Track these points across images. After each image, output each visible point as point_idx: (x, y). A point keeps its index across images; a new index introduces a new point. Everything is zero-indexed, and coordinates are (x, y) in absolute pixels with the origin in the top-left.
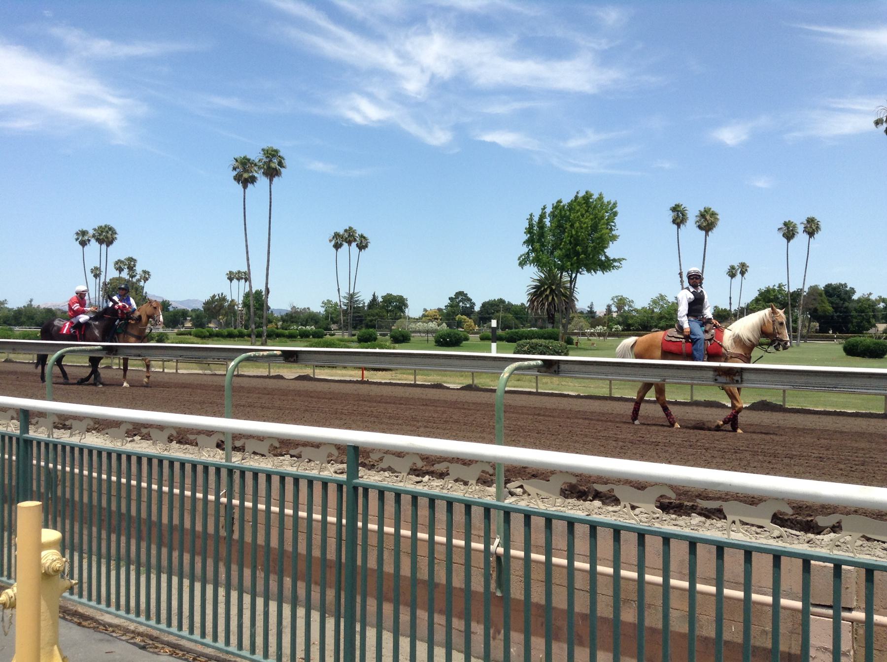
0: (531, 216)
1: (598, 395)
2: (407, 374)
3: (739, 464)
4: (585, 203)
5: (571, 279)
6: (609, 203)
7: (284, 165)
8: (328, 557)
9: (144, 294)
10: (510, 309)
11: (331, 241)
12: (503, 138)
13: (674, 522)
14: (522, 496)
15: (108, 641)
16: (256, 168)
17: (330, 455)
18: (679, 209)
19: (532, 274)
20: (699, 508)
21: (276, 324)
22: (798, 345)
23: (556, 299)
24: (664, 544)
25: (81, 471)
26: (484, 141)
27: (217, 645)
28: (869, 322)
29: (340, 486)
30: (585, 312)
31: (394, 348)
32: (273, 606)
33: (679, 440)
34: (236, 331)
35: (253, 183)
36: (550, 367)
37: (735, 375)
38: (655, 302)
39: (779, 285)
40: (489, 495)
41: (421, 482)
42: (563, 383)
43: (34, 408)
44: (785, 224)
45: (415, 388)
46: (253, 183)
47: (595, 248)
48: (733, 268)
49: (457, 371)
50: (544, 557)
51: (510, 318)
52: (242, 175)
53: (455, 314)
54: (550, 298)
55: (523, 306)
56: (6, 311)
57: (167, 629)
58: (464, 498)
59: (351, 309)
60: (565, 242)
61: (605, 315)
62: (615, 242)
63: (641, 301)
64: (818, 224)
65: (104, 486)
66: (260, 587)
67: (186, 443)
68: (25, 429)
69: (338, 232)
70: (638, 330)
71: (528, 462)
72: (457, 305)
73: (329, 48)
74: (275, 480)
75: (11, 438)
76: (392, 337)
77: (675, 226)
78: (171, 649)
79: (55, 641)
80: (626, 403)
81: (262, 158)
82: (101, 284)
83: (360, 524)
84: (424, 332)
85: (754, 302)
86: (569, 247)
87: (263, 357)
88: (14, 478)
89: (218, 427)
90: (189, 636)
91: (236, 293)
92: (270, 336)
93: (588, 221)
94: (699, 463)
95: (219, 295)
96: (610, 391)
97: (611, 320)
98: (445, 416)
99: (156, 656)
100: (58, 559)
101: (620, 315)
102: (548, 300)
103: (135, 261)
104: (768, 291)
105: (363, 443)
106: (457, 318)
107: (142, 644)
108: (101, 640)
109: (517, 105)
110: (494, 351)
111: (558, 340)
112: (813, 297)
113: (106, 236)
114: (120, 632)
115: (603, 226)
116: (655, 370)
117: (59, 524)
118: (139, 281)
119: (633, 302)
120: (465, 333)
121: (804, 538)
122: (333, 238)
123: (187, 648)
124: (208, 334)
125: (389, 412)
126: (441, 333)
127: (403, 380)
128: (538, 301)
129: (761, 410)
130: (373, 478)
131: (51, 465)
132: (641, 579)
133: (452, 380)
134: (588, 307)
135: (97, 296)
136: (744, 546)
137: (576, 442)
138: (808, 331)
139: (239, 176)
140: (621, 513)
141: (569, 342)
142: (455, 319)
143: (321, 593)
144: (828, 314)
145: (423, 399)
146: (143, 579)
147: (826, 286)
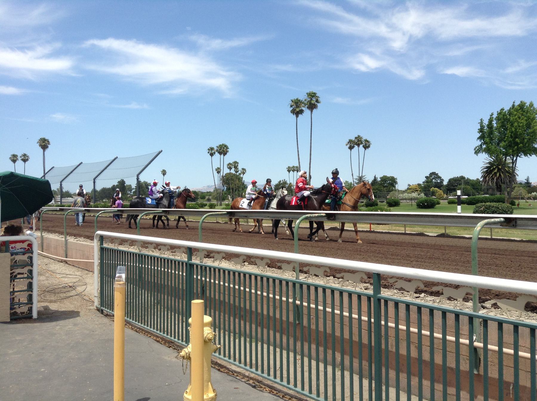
0: (481, 121)
2: (399, 227)
10: (468, 182)
11: (346, 145)
12: (459, 71)
14: (491, 309)
15: (235, 381)
16: (303, 105)
17: (325, 271)
23: (502, 175)
25: (215, 281)
26: (447, 74)
27: (297, 389)
30: (523, 183)
31: (390, 211)
36: (510, 223)
40: (468, 308)
42: (510, 232)
45: (405, 236)
47: (530, 139)
51: (469, 189)
54: (498, 175)
55: (478, 181)
57: (268, 377)
60: (508, 137)
66: (321, 356)
67: (273, 267)
68: (190, 258)
69: (351, 139)
71: (492, 286)
73: (344, 28)
74: (328, 292)
75: (183, 263)
78: (270, 389)
79: (210, 380)
82: (221, 177)
83: (383, 323)
84: (409, 199)
88: (184, 285)
89: (266, 256)
90: (280, 382)
98: (429, 254)
99: (261, 392)
100: (211, 333)
102: (496, 176)
103: (238, 163)
105: (383, 272)
106: (431, 190)
107: (254, 384)
108: (232, 381)
109: (469, 49)
110: (459, 211)
111: (504, 203)
116: (427, 219)
117: (212, 314)
118: (240, 174)
120: (438, 199)
122: (348, 143)
123: (279, 389)
125: (391, 251)
126: (420, 199)
127: (396, 230)
128: (489, 177)
130: (387, 293)
134: (525, 180)
135: (219, 183)
136: (406, 302)
137: (524, 272)
141: (513, 204)
142: (430, 190)
145: (412, 243)
146: (254, 344)
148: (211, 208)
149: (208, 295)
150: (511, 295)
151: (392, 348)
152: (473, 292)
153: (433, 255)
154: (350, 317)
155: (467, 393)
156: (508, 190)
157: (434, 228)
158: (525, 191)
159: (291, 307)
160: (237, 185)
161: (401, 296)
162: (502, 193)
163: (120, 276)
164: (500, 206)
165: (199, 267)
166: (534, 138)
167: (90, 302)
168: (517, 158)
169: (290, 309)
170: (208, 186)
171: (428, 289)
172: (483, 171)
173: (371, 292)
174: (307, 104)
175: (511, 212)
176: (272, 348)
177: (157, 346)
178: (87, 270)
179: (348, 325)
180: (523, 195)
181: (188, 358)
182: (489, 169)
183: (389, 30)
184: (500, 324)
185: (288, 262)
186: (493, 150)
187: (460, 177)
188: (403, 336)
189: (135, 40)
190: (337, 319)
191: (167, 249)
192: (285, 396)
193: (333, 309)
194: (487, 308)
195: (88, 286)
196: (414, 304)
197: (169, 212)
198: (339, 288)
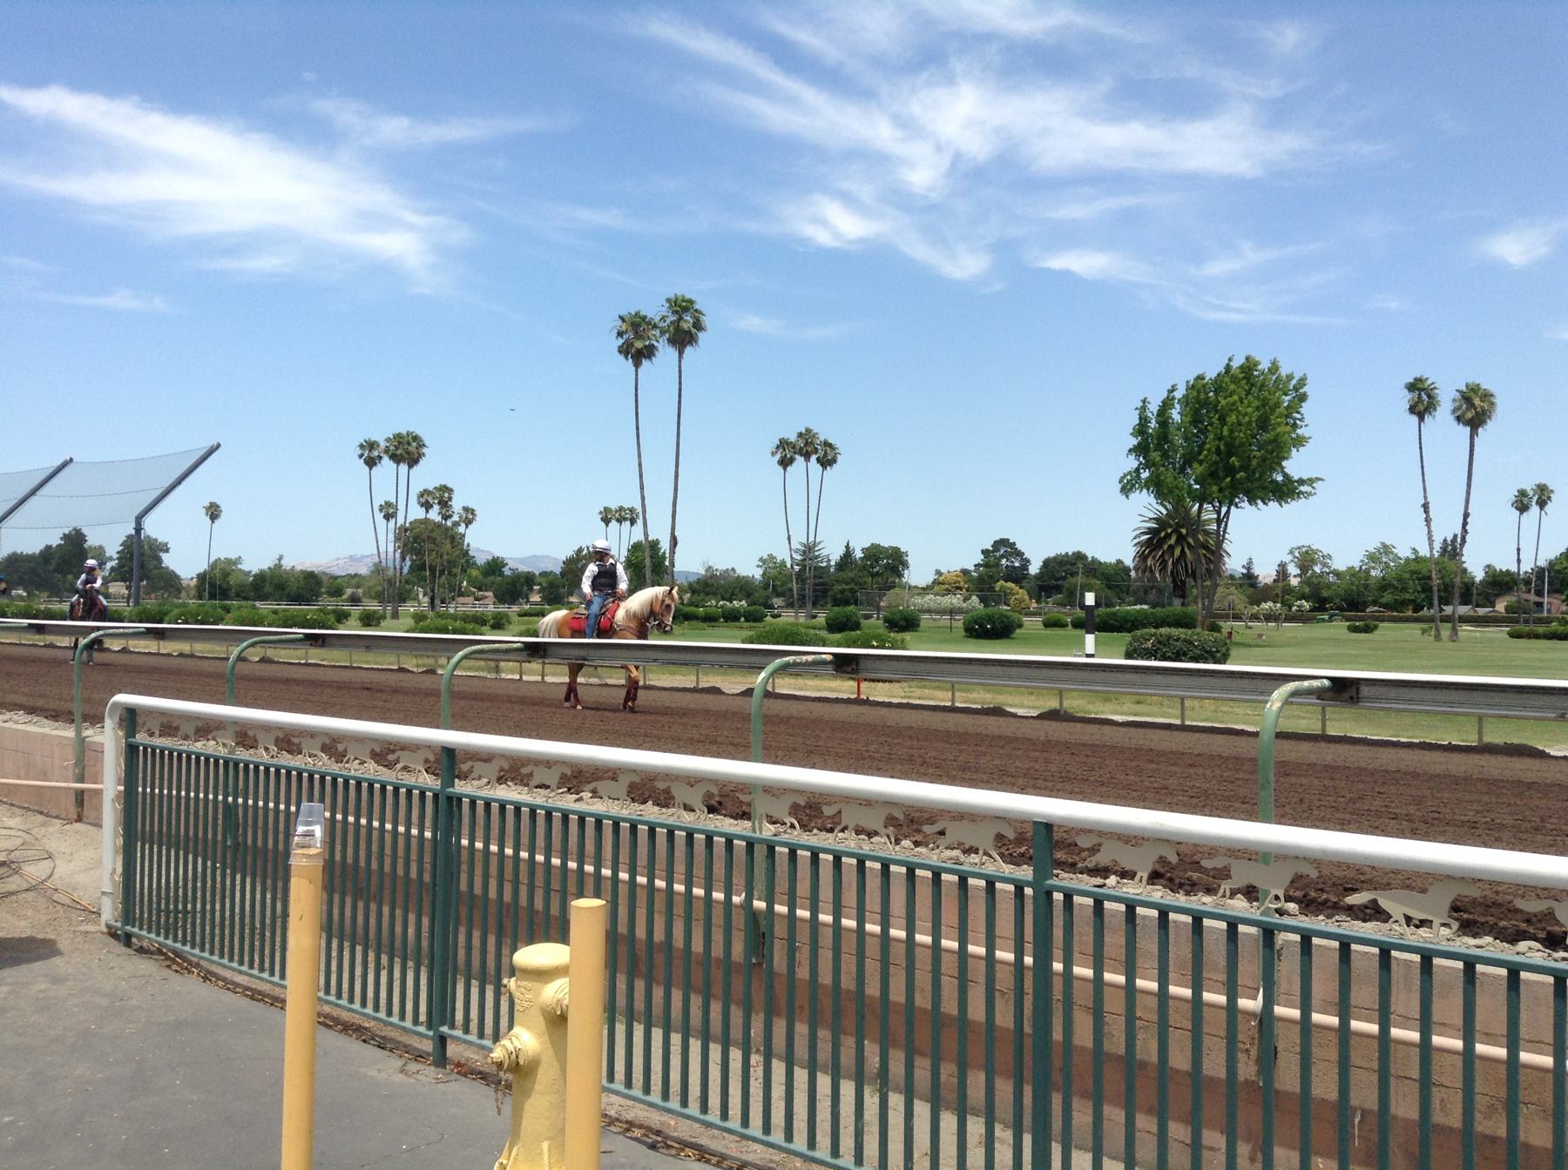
2: (929, 689)
4: (1246, 377)
6: (1290, 377)
11: (773, 454)
12: (1084, 263)
16: (657, 333)
18: (1421, 386)
19: (1145, 507)
26: (1049, 269)
38: (1372, 557)
41: (1105, 885)
47: (1264, 459)
48: (1522, 493)
49: (1025, 687)
52: (632, 345)
53: (993, 579)
54: (1177, 552)
56: (242, 577)
60: (1209, 450)
61: (1275, 581)
62: (1301, 449)
66: (801, 1050)
72: (998, 565)
73: (775, 117)
76: (886, 620)
77: (1415, 419)
78: (696, 1152)
85: (1564, 558)
87: (807, 664)
93: (1250, 410)
96: (1324, 726)
97: (1288, 590)
101: (1306, 582)
102: (1173, 554)
103: (450, 491)
105: (1063, 818)
106: (998, 586)
113: (407, 451)
115: (1279, 420)
118: (456, 524)
119: (1330, 557)
122: (778, 447)
126: (975, 613)
128: (1154, 557)
133: (1016, 700)
134: (1243, 567)
140: (1492, 949)
142: (993, 588)
157: (1022, 694)
158: (1243, 598)
159: (739, 920)
160: (445, 557)
163: (307, 831)
167: (78, 912)
172: (1137, 540)
174: (668, 331)
175: (1224, 654)
176: (676, 1039)
178: (41, 813)
179: (904, 965)
181: (514, 1065)
183: (899, 134)
186: (1170, 485)
187: (1074, 554)
189: (136, 98)
190: (872, 949)
194: (1289, 915)
195: (58, 862)
197: (324, 641)
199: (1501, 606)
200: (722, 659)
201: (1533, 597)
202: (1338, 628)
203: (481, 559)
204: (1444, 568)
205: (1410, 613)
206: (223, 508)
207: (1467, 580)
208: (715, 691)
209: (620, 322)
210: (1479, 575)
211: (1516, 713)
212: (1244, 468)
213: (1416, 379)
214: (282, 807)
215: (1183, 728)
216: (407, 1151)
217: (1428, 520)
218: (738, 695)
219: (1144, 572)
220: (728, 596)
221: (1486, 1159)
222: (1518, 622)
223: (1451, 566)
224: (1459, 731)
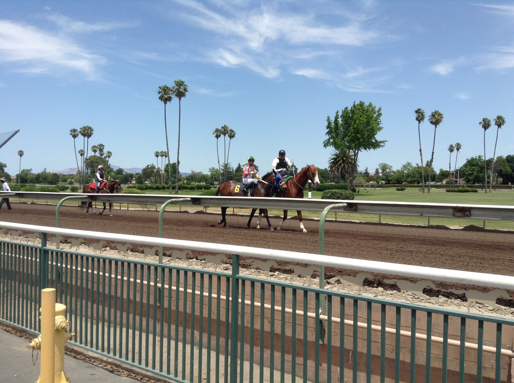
0: (328, 118)
1: (372, 222)
3: (463, 264)
5: (355, 154)
7: (187, 90)
8: (180, 310)
9: (109, 165)
11: (214, 134)
12: (308, 73)
13: (428, 301)
15: (91, 367)
18: (420, 112)
19: (331, 151)
20: (442, 292)
21: (183, 182)
22: (490, 192)
23: (346, 165)
24: (428, 316)
25: (77, 268)
26: (297, 75)
27: (155, 371)
28: (17, 179)
29: (228, 279)
30: (363, 173)
32: (188, 347)
33: (425, 250)
34: (161, 186)
35: (170, 101)
36: (352, 208)
37: (466, 212)
38: (405, 167)
39: (479, 156)
41: (274, 275)
43: (50, 232)
44: (484, 120)
46: (170, 101)
47: (369, 135)
48: (451, 146)
50: (353, 322)
54: (342, 165)
55: (326, 170)
57: (126, 361)
58: (303, 287)
59: (226, 173)
61: (375, 175)
62: (380, 131)
63: (396, 166)
64: (503, 120)
65: (90, 277)
66: (181, 336)
67: (136, 251)
68: (44, 244)
70: (394, 183)
73: (205, 24)
74: (190, 274)
75: (36, 249)
78: (128, 373)
79: (62, 369)
80: (390, 227)
81: (174, 86)
83: (240, 300)
85: (464, 166)
86: (353, 135)
87: (180, 201)
88: (38, 271)
90: (138, 366)
91: (161, 164)
92: (180, 188)
93: (364, 119)
94: (438, 263)
95: (151, 165)
97: (379, 177)
99: (119, 377)
103: (103, 146)
104: (473, 159)
105: (242, 253)
107: (111, 369)
108: (88, 367)
109: (316, 54)
111: (347, 190)
112: (500, 163)
114: (98, 362)
115: (373, 122)
118: (106, 157)
119: (392, 167)
121: (509, 311)
122: (215, 131)
124: (145, 187)
129: (470, 231)
130: (245, 273)
131: (59, 265)
132: (369, 327)
134: (365, 170)
135: (82, 166)
138: (496, 183)
139: (162, 97)
140: (396, 295)
141: (354, 191)
143: (217, 341)
144: (508, 173)
146: (112, 330)
147: (507, 156)
148: (73, 191)
149: (64, 280)
150: (351, 271)
151: (248, 324)
152: (319, 270)
153: (287, 236)
154: (210, 296)
155: (313, 361)
156: (351, 178)
159: (152, 290)
161: (257, 274)
162: (345, 181)
164: (343, 192)
165: (54, 253)
166: (373, 134)
168: (358, 151)
169: (151, 292)
170: (70, 168)
171: (281, 267)
172: (329, 162)
173: (230, 272)
175: (352, 198)
176: (137, 333)
177: (7, 336)
180: (363, 183)
182: (335, 160)
184: (342, 298)
185: (150, 246)
188: (257, 312)
190: (197, 299)
191: (18, 235)
192: (143, 378)
193: (194, 290)
194: (331, 284)
196: (269, 283)
197: (23, 196)
198: (200, 270)
199: (444, 182)
200: (155, 200)
201: (454, 179)
202: (393, 190)
203: (115, 169)
204: (427, 170)
205: (416, 184)
206: (24, 152)
207: (434, 174)
208: (186, 212)
209: (159, 89)
210: (438, 172)
211: (407, 214)
212: (362, 138)
213: (418, 109)
214: (6, 254)
215: (336, 221)
216: (16, 377)
217: (421, 155)
218: (194, 213)
219: (332, 172)
220: (199, 181)
221: (391, 367)
222: (449, 187)
223: (429, 169)
224: (424, 221)
